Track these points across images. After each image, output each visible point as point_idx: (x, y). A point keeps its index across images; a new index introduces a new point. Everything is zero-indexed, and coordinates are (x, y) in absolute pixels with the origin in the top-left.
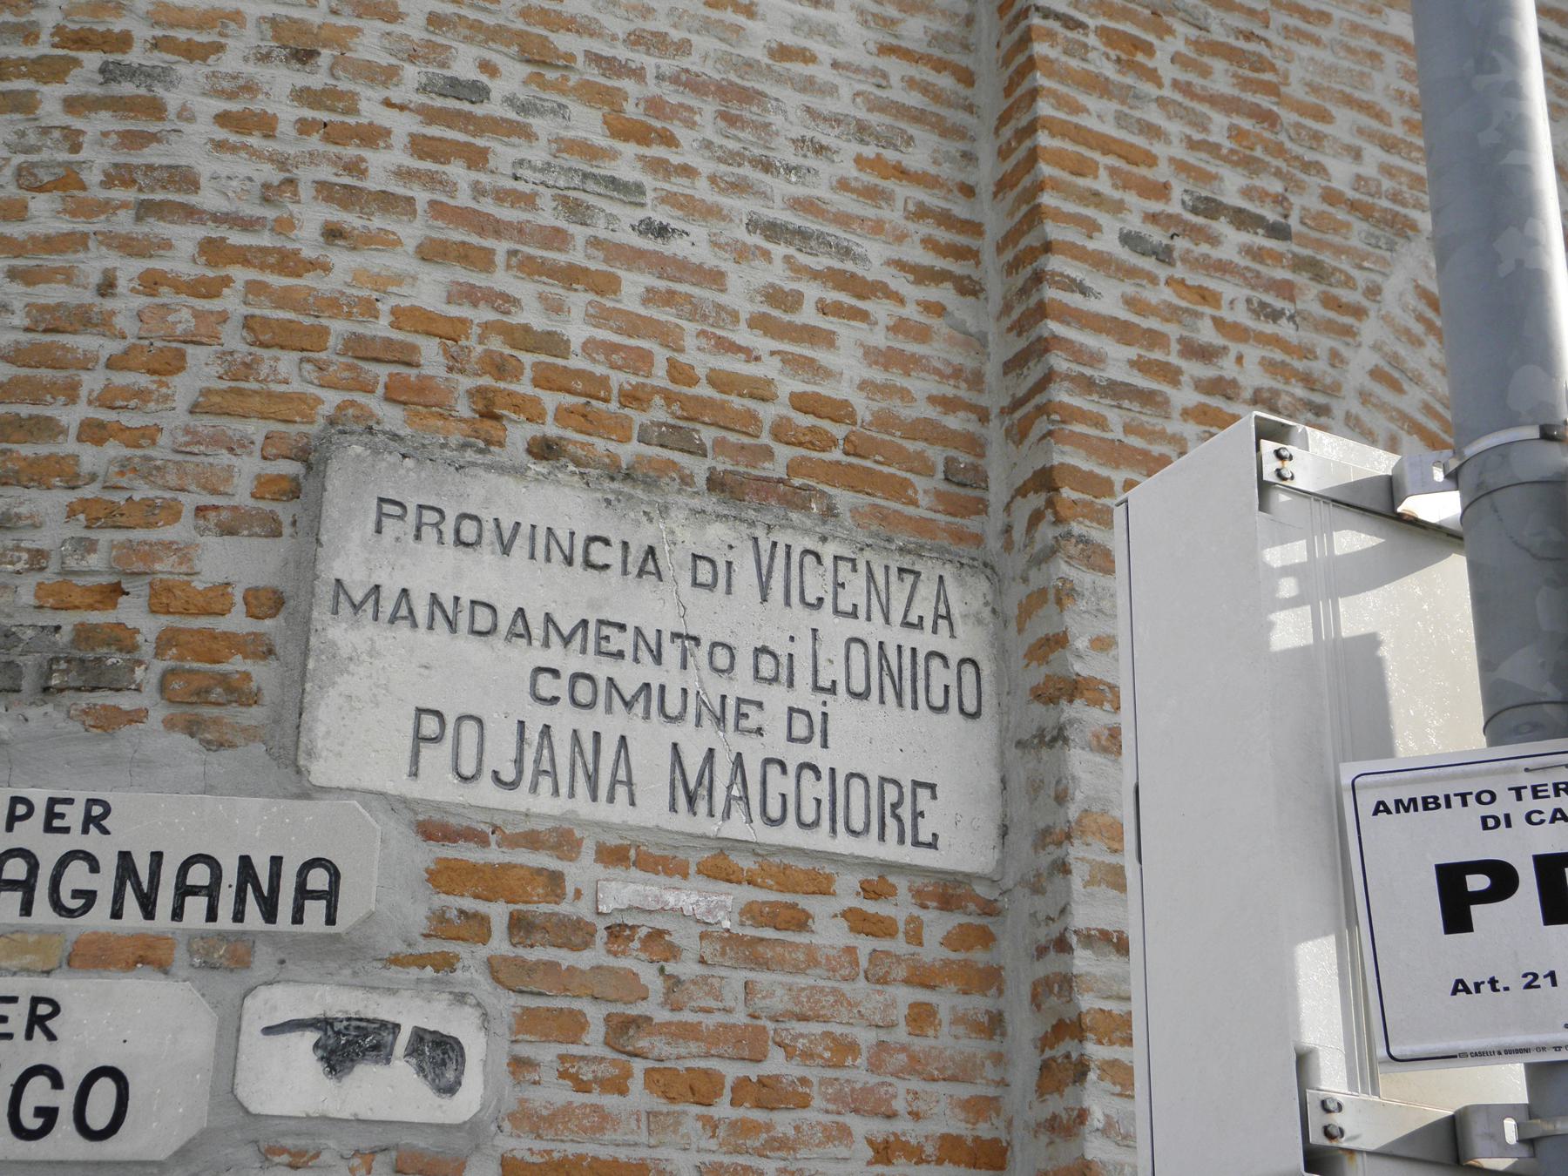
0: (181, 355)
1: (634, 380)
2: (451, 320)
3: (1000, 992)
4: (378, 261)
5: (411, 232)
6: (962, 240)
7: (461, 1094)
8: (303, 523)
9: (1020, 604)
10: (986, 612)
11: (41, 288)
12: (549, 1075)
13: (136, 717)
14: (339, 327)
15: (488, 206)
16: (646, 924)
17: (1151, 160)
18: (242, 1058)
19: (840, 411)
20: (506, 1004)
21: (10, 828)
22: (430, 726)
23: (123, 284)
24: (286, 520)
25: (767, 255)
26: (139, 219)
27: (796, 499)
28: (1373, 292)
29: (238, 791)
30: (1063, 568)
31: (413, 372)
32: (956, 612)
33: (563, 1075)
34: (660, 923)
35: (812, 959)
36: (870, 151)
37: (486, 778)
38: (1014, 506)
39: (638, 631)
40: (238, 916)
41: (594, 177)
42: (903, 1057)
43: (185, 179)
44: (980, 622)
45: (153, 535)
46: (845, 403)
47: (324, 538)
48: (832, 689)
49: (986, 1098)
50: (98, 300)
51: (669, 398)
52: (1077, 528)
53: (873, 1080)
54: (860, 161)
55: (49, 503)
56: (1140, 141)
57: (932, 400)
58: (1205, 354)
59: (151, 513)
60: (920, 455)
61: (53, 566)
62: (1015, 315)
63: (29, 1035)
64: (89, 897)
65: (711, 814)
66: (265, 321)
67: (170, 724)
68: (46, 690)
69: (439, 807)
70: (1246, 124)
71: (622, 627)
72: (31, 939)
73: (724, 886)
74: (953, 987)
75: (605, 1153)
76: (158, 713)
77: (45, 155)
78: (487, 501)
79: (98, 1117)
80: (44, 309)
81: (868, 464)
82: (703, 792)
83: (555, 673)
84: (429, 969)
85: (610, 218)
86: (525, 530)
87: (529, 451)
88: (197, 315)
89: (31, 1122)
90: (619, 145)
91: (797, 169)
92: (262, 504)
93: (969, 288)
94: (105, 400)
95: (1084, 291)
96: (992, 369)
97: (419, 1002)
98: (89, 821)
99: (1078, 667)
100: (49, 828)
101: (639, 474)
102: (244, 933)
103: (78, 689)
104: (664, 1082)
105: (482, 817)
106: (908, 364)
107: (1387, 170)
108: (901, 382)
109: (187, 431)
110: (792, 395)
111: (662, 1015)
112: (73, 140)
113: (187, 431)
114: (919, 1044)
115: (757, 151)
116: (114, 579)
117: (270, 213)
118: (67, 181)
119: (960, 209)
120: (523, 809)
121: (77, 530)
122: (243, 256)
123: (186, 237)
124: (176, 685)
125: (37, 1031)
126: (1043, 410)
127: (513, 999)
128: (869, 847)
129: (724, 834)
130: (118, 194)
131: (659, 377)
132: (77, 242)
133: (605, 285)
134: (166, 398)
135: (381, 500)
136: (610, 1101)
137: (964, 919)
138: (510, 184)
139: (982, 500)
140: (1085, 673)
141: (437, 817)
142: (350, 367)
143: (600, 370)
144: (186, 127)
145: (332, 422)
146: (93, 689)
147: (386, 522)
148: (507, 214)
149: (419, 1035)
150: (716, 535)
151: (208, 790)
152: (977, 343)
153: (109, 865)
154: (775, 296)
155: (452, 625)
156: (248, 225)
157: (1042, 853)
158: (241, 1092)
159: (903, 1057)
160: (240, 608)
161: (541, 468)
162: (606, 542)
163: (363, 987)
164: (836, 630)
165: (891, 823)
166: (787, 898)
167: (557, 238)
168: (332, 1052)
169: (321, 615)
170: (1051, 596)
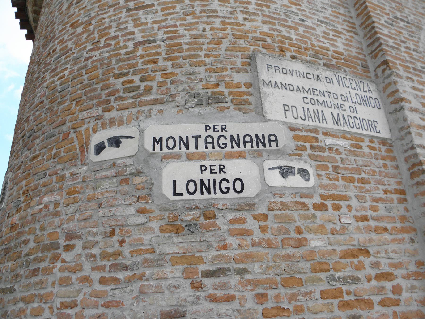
0: (222, 41)
1: (306, 46)
2: (271, 34)
3: (397, 161)
4: (255, 24)
5: (260, 19)
6: (352, 26)
7: (310, 181)
8: (253, 70)
9: (383, 87)
10: (376, 90)
11: (191, 32)
12: (324, 178)
13: (228, 108)
14: (250, 35)
15: (272, 15)
16: (335, 148)
17: (385, 9)
18: (265, 175)
19: (341, 54)
20: (313, 163)
21: (206, 131)
22: (287, 108)
23: (207, 30)
24: (249, 70)
25: (322, 26)
26: (208, 18)
27: (339, 68)
28: (419, 38)
29: (252, 122)
30: (393, 78)
31: (266, 43)
32: (372, 89)
33: (327, 177)
34: (337, 147)
35: (364, 155)
36: (333, 10)
37: (299, 118)
38: (377, 70)
39: (320, 91)
40: (258, 146)
41: (290, 11)
42: (384, 173)
43: (216, 11)
44: (376, 91)
45: (223, 74)
46: (342, 52)
47: (259, 71)
48: (355, 103)
49: (399, 181)
50: (203, 33)
51: (312, 49)
52: (394, 71)
53: (380, 178)
54: (332, 11)
55: (201, 69)
56: (382, 6)
57: (356, 52)
58: (404, 42)
59: (222, 70)
60: (356, 62)
61: (205, 80)
62: (368, 36)
63: (220, 173)
64: (226, 144)
65: (341, 126)
66: (236, 34)
67: (235, 109)
68: (208, 104)
69: (292, 124)
70: (397, 5)
71: (316, 90)
72: (216, 153)
73: (346, 140)
74: (389, 160)
75: (338, 193)
76: (232, 107)
77: (187, 9)
78: (286, 66)
79: (238, 188)
80: (193, 35)
81: (348, 63)
82: (339, 122)
83: (307, 98)
84: (297, 156)
85: (294, 18)
86: (295, 71)
87: (291, 57)
88: (223, 34)
89: (225, 190)
90: (292, 6)
91: (322, 12)
92: (243, 67)
93: (356, 34)
94: (208, 50)
95: (382, 30)
96: (364, 47)
97: (297, 163)
98: (222, 129)
99: (402, 95)
100: (214, 131)
101: (311, 62)
102: (260, 150)
103: (215, 103)
104: (344, 179)
105: (300, 126)
106: (351, 46)
107: (415, 18)
108: (350, 49)
109: (226, 54)
110: (333, 50)
111: (342, 166)
112: (193, 7)
113: (226, 54)
114: (387, 171)
115: (315, 8)
116: (217, 82)
117: (233, 16)
118: (193, 13)
119: (351, 20)
120: (307, 124)
121: (208, 73)
122: (229, 24)
123: (218, 21)
124: (235, 101)
125: (221, 171)
126: (380, 51)
127: (315, 162)
128: (368, 133)
129: (344, 130)
130: (203, 14)
131: (310, 46)
132: (197, 23)
133: (296, 29)
134: (220, 49)
135: (267, 65)
136: (336, 183)
137: (387, 147)
138: (275, 11)
139: (368, 71)
140: (403, 96)
141: (292, 126)
142: (254, 42)
143: (299, 44)
144: (214, 3)
145: (253, 52)
146: (218, 103)
147: (269, 69)
148: (276, 16)
149: (299, 169)
150: (328, 73)
151: (246, 122)
152: (360, 43)
153: (229, 138)
154: (325, 33)
155: (286, 88)
156: (229, 18)
157: (402, 132)
158: (267, 182)
159: (384, 173)
160: (243, 86)
161: (294, 60)
162: (310, 74)
163: (286, 160)
164: (353, 92)
165: (371, 128)
166: (357, 143)
167: (285, 20)
168: (283, 173)
169: (261, 86)
170: (393, 83)
